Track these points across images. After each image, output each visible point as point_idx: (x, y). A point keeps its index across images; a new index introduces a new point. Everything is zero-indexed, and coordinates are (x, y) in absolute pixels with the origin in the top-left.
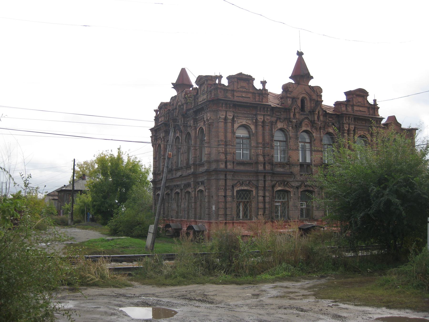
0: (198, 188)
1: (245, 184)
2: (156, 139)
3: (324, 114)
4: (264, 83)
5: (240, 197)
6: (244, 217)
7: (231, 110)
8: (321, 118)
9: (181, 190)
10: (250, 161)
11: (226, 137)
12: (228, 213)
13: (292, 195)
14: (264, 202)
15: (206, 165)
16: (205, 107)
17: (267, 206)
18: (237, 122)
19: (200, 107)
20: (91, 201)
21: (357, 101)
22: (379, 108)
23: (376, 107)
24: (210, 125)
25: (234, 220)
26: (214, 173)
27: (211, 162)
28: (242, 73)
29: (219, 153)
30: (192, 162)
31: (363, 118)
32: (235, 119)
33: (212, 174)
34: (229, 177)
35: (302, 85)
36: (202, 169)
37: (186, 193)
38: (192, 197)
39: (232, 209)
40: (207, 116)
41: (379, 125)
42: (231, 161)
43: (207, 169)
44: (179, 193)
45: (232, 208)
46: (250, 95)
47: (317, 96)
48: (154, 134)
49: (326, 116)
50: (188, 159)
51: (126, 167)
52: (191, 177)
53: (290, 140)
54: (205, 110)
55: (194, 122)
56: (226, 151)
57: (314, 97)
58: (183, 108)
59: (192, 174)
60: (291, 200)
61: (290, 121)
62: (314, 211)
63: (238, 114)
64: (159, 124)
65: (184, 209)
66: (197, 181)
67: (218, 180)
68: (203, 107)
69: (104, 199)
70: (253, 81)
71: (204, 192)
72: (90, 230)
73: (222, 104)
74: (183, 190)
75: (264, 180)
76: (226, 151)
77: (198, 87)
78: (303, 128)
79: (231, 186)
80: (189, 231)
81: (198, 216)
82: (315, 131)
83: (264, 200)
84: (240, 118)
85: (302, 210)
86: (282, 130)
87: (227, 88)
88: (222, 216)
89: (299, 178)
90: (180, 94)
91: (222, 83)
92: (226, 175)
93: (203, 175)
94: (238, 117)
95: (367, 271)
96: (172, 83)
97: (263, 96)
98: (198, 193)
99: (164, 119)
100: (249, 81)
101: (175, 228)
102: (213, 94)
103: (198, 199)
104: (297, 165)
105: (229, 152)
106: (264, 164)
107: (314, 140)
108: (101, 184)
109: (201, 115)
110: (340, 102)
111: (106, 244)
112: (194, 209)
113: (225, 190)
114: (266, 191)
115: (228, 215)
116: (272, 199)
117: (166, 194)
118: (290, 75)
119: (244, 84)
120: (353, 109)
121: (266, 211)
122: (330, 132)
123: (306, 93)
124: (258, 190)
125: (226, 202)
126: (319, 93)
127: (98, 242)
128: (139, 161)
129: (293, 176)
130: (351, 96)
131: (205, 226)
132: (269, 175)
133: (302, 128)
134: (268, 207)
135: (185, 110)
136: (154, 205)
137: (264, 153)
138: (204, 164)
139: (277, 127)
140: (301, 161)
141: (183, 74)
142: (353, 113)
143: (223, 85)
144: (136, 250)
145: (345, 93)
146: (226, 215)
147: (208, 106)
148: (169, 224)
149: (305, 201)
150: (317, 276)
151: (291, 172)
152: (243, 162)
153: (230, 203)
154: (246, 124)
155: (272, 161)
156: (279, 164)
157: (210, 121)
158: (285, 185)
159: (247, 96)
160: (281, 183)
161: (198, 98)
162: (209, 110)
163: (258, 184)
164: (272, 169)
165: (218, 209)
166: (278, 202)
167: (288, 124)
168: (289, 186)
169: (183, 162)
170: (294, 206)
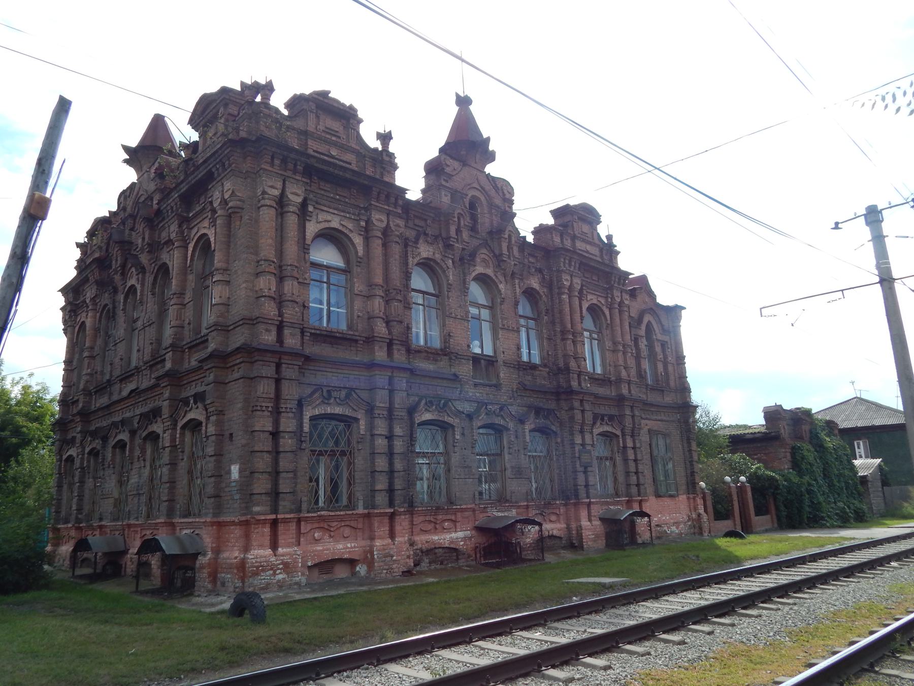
0: (183, 417)
1: (335, 398)
2: (74, 311)
4: (385, 138)
6: (331, 501)
9: (133, 433)
10: (352, 333)
11: (280, 253)
12: (284, 487)
13: (458, 437)
14: (391, 454)
16: (217, 169)
17: (398, 465)
18: (314, 217)
22: (618, 253)
27: (230, 328)
28: (329, 92)
30: (170, 341)
32: (311, 208)
33: (231, 364)
34: (288, 372)
35: (472, 167)
37: (145, 439)
42: (296, 326)
45: (295, 472)
55: (180, 226)
57: (498, 201)
60: (456, 449)
73: (273, 158)
78: (477, 268)
79: (296, 402)
80: (144, 558)
81: (178, 506)
83: (391, 447)
84: (325, 209)
88: (264, 497)
90: (145, 175)
92: (278, 366)
94: (317, 203)
101: (106, 550)
103: (183, 452)
104: (466, 357)
107: (502, 303)
112: (168, 485)
113: (277, 413)
115: (281, 495)
117: (90, 453)
119: (336, 125)
122: (534, 287)
123: (480, 188)
133: (475, 266)
139: (419, 254)
146: (275, 495)
148: (86, 539)
151: (455, 375)
152: (333, 334)
153: (289, 454)
154: (341, 228)
157: (230, 204)
159: (342, 158)
165: (249, 474)
168: (451, 410)
169: (141, 352)
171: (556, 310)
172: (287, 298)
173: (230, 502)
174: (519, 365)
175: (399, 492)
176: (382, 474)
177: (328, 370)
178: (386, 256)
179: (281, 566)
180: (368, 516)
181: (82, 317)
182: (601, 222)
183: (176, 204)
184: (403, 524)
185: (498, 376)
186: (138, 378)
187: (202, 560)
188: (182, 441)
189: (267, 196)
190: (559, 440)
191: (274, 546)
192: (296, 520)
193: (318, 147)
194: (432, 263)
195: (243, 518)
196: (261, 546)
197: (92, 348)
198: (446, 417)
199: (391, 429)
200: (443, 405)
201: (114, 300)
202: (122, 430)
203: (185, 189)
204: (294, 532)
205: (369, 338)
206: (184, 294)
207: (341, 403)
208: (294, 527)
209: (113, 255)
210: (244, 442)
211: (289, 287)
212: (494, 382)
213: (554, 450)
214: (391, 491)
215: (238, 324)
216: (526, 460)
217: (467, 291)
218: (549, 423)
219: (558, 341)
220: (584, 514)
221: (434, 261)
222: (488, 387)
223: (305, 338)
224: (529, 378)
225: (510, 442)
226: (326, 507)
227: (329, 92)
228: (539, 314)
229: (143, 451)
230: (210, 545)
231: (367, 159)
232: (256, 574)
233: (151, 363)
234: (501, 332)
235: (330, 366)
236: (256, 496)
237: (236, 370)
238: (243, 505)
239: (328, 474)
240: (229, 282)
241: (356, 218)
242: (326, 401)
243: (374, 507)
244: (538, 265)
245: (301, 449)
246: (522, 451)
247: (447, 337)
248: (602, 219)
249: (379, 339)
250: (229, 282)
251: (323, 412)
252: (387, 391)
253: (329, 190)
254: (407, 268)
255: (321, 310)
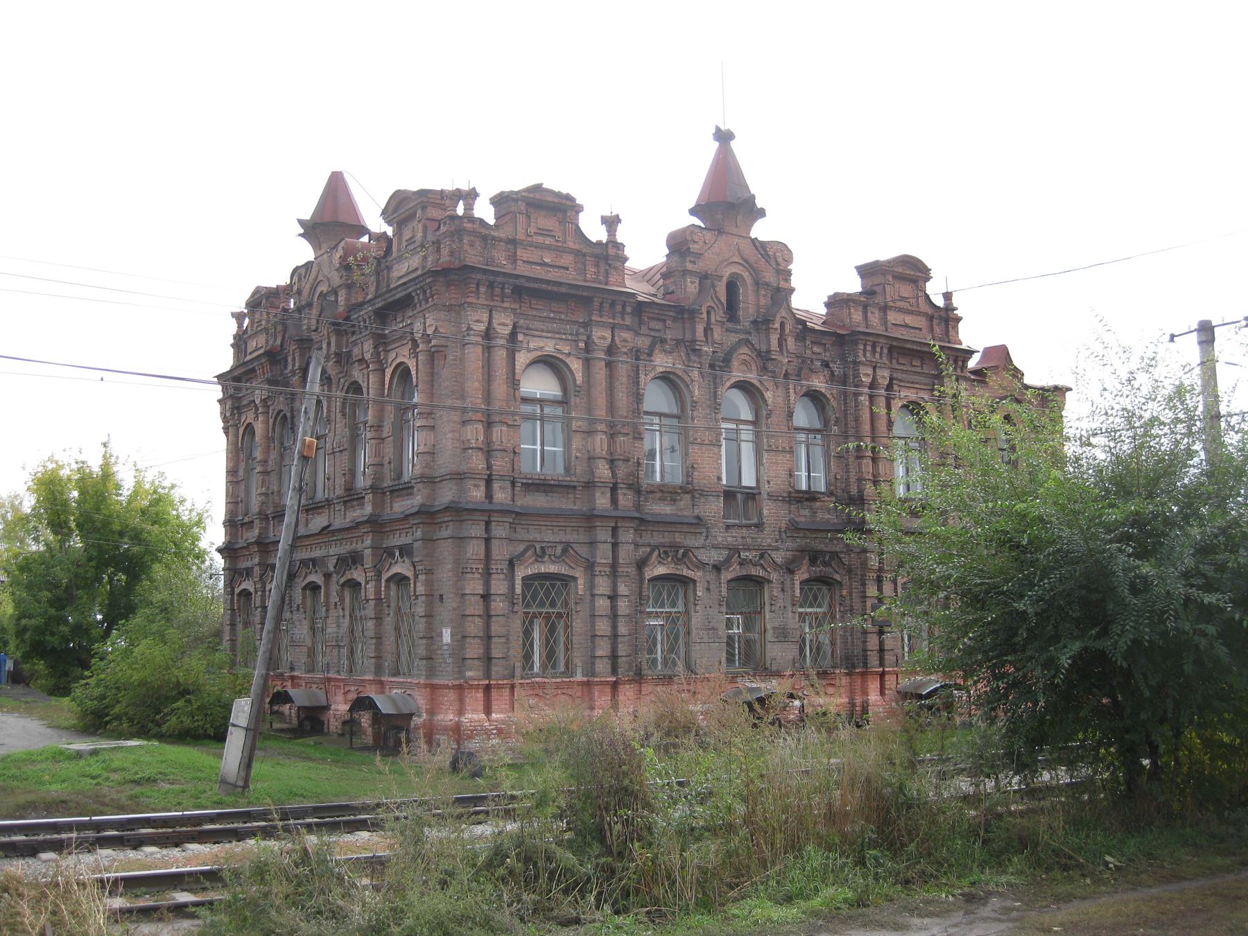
0: (388, 570)
1: (550, 556)
2: (238, 408)
3: (798, 331)
5: (534, 597)
7: (506, 305)
8: (791, 343)
9: (327, 576)
10: (569, 479)
11: (488, 396)
12: (496, 653)
13: (699, 594)
14: (614, 616)
15: (419, 490)
16: (418, 295)
17: (623, 629)
19: (398, 296)
20: (11, 616)
21: (897, 294)
22: (959, 319)
23: (951, 316)
24: (432, 356)
25: (513, 677)
26: (450, 518)
28: (542, 184)
29: (465, 449)
30: (369, 483)
31: (915, 347)
32: (520, 337)
33: (439, 521)
34: (499, 531)
36: (401, 506)
37: (343, 585)
38: (367, 601)
39: (508, 639)
40: (425, 323)
41: (962, 372)
43: (422, 505)
44: (319, 587)
45: (507, 637)
46: (567, 260)
47: (778, 272)
48: (231, 391)
49: (804, 339)
50: (352, 472)
51: (129, 502)
52: (365, 530)
53: (692, 410)
54: (418, 305)
55: (376, 347)
56: (488, 442)
57: (769, 276)
58: (336, 301)
59: (366, 522)
60: (698, 608)
61: (695, 350)
62: (769, 646)
63: (527, 322)
64: (249, 358)
65: (337, 641)
66: (384, 546)
67: (460, 540)
68: (410, 293)
69: (57, 610)
70: (577, 213)
71: (412, 582)
72: (7, 712)
73: (478, 285)
74: (335, 578)
75: (613, 541)
76: (488, 442)
77: (390, 231)
82: (770, 385)
83: (614, 608)
85: (730, 640)
86: (667, 378)
87: (493, 233)
88: (476, 662)
89: (722, 537)
90: (325, 256)
91: (476, 216)
92: (488, 524)
93: (407, 526)
94: (528, 329)
95: (1106, 864)
96: (298, 220)
97: (610, 265)
98: (387, 587)
99: (267, 343)
100: (565, 212)
101: (307, 704)
102: (445, 251)
103: (389, 606)
104: (713, 494)
105: (499, 447)
106: (614, 489)
107: (769, 415)
108: (46, 560)
109: (403, 321)
110: (845, 297)
111: (71, 768)
112: (374, 641)
113: (487, 574)
114: (619, 580)
115: (493, 660)
116: (636, 606)
118: (692, 204)
120: (884, 321)
121: (620, 646)
123: (742, 262)
124: (593, 576)
125: (488, 616)
126: (783, 264)
127: (42, 761)
128: (173, 486)
129: (704, 530)
130: (878, 279)
131: (413, 698)
132: (627, 525)
134: (627, 633)
135: (341, 309)
136: (229, 627)
137: (611, 453)
138: (413, 487)
140: (724, 482)
141: (336, 189)
142: (886, 331)
143: (481, 221)
144: (184, 792)
145: (859, 268)
146: (488, 659)
147: (428, 291)
149: (741, 613)
150: (951, 898)
151: (698, 517)
152: (546, 482)
153: (500, 618)
155: (638, 478)
156: (661, 491)
157: (434, 342)
158: (678, 561)
159: (557, 264)
160: (666, 553)
161: (389, 268)
162: (430, 304)
163: (594, 555)
164: (638, 507)
165: (461, 638)
166: (657, 615)
167: (689, 360)
168: (692, 562)
169: (331, 481)
170: (706, 629)
171: (850, 418)
172: (496, 447)
173: (443, 665)
174: (789, 497)
175: (624, 659)
176: (604, 638)
177: (541, 523)
178: (611, 378)
179: (495, 731)
180: (588, 684)
181: (248, 417)
182: (932, 277)
183: (370, 317)
184: (628, 693)
185: (760, 514)
186: (329, 511)
187: (417, 721)
188: (388, 595)
189: (472, 332)
190: (844, 592)
191: (488, 711)
192: (509, 686)
193: (528, 255)
194: (671, 376)
195: (456, 683)
196: (475, 711)
197: (265, 461)
198: (685, 570)
199: (614, 587)
200: (682, 555)
201: (292, 407)
202: (314, 570)
203: (380, 305)
204: (507, 698)
205: (589, 483)
206: (383, 426)
207: (556, 559)
208: (507, 694)
209: (289, 352)
210: (455, 605)
211: (498, 433)
212: (755, 521)
213: (837, 606)
214: (614, 657)
215: (445, 478)
216: (794, 618)
217: (718, 407)
218: (831, 570)
219: (851, 460)
220: (874, 686)
221: (674, 374)
222: (744, 529)
223: (516, 488)
224: (806, 512)
225: (771, 598)
226: (541, 673)
227: (542, 184)
228: (826, 423)
229: (342, 599)
230: (424, 707)
231: (588, 258)
232: (471, 737)
233: (345, 499)
234: (765, 455)
235: (544, 519)
236: (469, 661)
237: (444, 527)
238: (457, 669)
239: (543, 637)
240: (434, 427)
241: (574, 338)
242: (540, 560)
243: (593, 675)
244: (827, 356)
245: (513, 612)
246: (790, 608)
247: (690, 470)
248: (932, 273)
249: (600, 485)
250: (434, 427)
251: (536, 571)
252: (610, 546)
253: (541, 307)
254: (638, 389)
255: (536, 450)
